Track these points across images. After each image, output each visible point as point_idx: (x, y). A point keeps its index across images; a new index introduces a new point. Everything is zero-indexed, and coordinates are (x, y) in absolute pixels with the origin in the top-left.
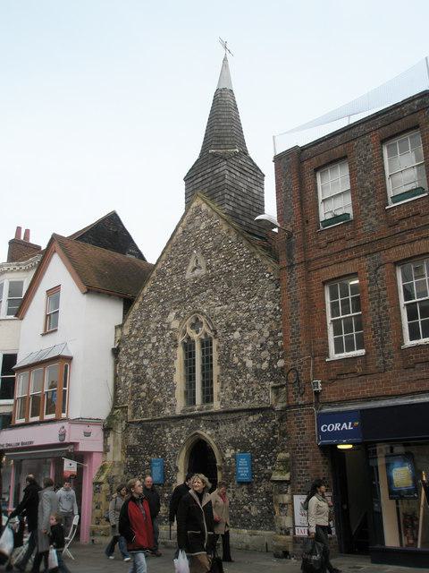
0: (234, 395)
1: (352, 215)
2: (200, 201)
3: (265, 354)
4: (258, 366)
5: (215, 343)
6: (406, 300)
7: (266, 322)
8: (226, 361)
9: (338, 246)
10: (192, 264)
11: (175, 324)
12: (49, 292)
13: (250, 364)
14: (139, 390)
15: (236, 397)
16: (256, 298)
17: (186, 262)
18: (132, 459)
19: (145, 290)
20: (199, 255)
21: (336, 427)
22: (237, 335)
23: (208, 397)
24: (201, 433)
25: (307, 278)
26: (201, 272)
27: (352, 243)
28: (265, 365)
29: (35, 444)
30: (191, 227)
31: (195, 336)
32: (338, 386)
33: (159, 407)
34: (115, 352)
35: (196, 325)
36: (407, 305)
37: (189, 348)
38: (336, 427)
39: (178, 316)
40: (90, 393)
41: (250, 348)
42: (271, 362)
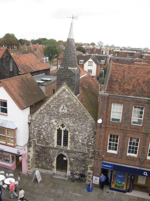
0: (75, 147)
1: (121, 120)
2: (65, 88)
3: (85, 140)
4: (83, 142)
5: (69, 133)
6: (129, 145)
7: (87, 133)
8: (73, 138)
9: (115, 127)
10: (62, 107)
11: (55, 124)
12: (5, 104)
13: (80, 141)
14: (40, 137)
15: (75, 148)
16: (84, 125)
17: (59, 106)
18: (37, 154)
19: (42, 108)
20: (64, 106)
21: (107, 166)
22: (77, 133)
23: (66, 143)
24: (63, 153)
25: (105, 132)
26: (66, 111)
27: (120, 128)
28: (85, 143)
29: (4, 150)
30: (61, 95)
31: (63, 129)
32: (108, 158)
33: (47, 144)
34: (29, 124)
35: (63, 126)
36: (129, 146)
37: (59, 131)
38: (107, 166)
39: (56, 121)
40: (22, 138)
41: (81, 137)
42: (87, 143)
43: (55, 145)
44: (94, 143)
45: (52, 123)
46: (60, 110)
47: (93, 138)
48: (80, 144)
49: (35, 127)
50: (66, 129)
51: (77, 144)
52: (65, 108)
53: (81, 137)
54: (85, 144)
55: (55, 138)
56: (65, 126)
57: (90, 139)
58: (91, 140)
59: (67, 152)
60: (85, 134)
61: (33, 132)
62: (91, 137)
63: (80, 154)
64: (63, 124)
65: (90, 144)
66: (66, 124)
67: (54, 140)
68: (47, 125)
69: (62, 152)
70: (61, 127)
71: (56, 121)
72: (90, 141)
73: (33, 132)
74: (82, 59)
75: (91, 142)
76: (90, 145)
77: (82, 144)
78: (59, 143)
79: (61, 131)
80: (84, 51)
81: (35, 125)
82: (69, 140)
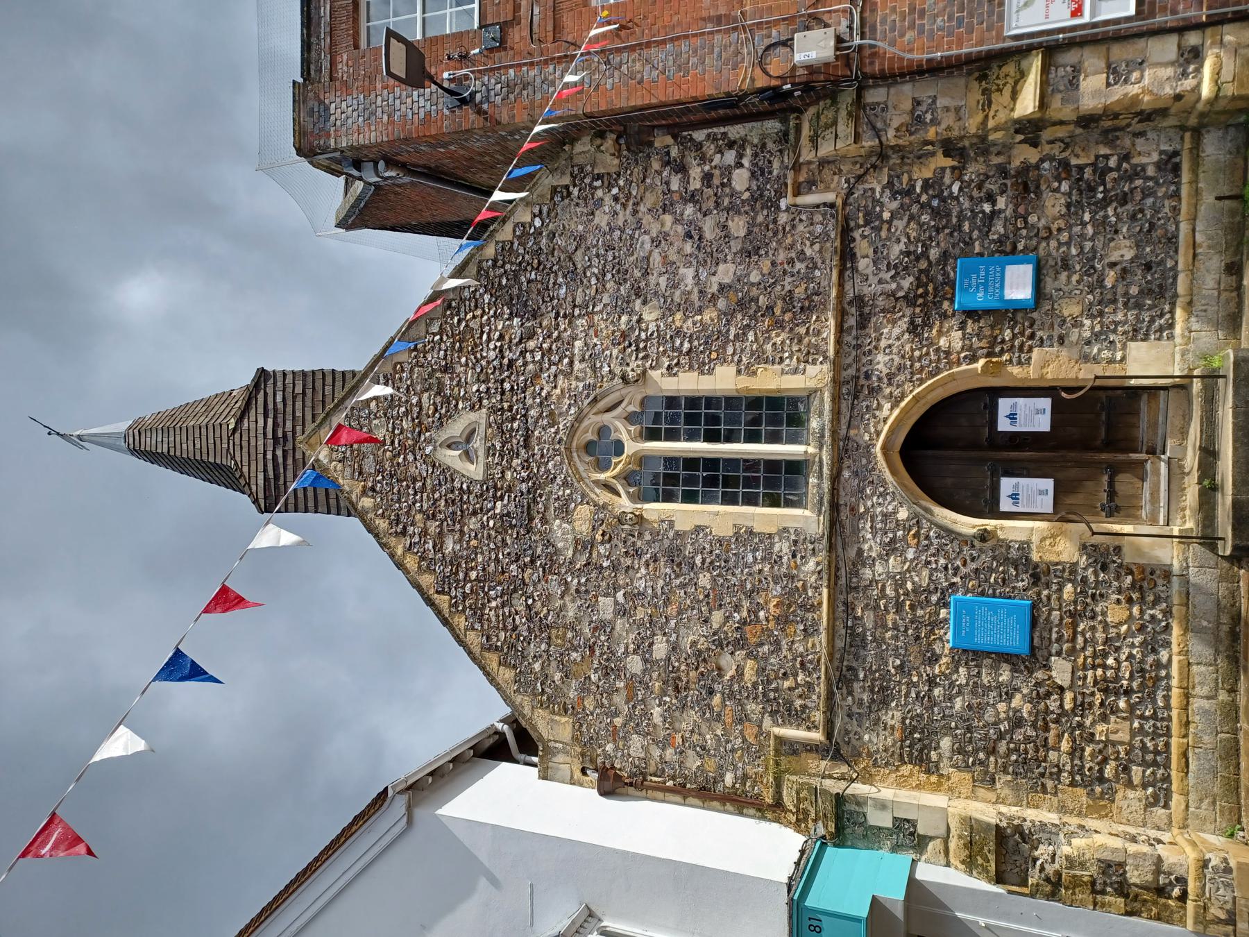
4: (736, 246)
10: (451, 457)
13: (726, 272)
23: (779, 414)
33: (794, 607)
43: (805, 518)
44: (731, 145)
45: (582, 545)
46: (475, 470)
47: (682, 169)
48: (755, 277)
49: (639, 722)
50: (630, 418)
51: (763, 301)
52: (456, 428)
53: (688, 274)
54: (751, 225)
55: (718, 517)
56: (603, 431)
57: (695, 184)
58: (707, 178)
59: (853, 388)
60: (656, 242)
61: (693, 763)
62: (675, 186)
63: (863, 264)
64: (589, 447)
65: (741, 180)
66: (579, 419)
67: (745, 537)
68: (610, 600)
69: (869, 446)
70: (619, 465)
71: (565, 511)
72: (715, 181)
73: (693, 763)
74: (995, 489)
75: (727, 171)
76: (758, 172)
77: (750, 252)
78: (778, 482)
79: (643, 459)
80: (1116, 116)
81: (618, 721)
82: (724, 380)
